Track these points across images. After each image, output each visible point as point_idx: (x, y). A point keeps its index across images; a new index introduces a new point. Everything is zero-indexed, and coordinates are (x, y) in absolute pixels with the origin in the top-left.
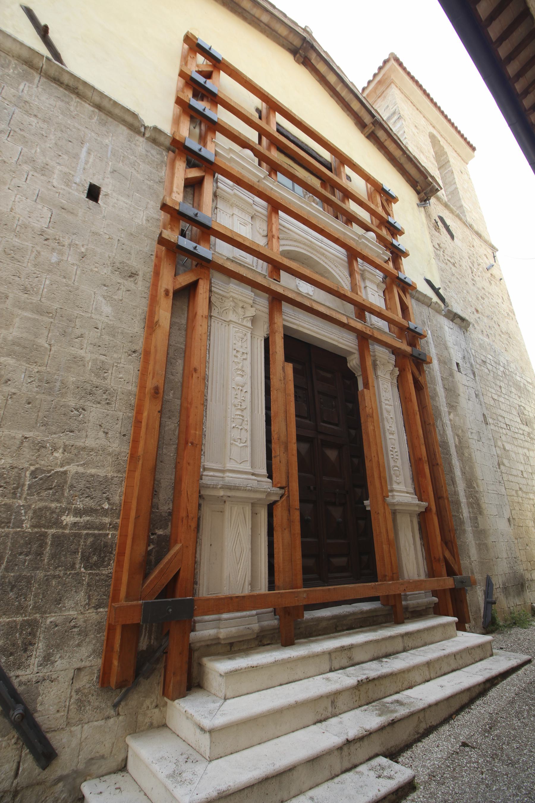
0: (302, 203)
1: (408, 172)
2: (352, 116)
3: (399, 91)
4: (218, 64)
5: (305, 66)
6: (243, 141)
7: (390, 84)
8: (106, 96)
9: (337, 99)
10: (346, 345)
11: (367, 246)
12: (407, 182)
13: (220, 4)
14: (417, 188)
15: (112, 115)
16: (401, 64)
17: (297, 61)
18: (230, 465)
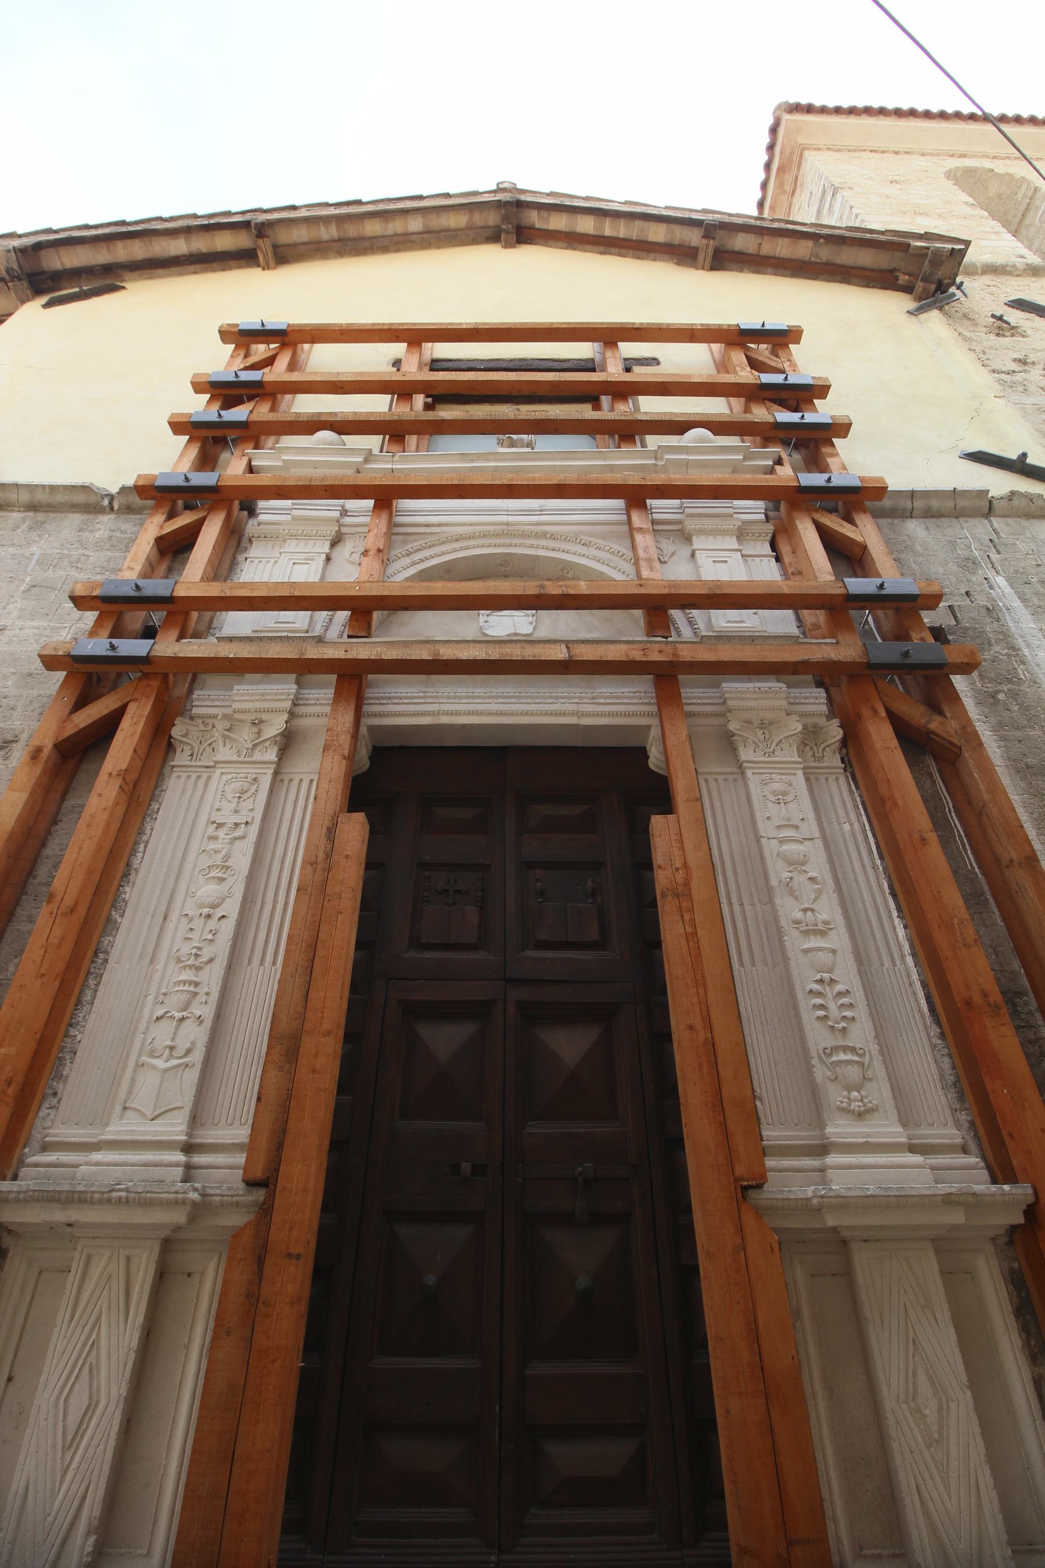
0: (472, 461)
1: (853, 268)
2: (664, 256)
3: (830, 153)
4: (286, 338)
5: (530, 244)
6: (307, 422)
7: (801, 155)
8: (36, 486)
9: (617, 250)
10: (610, 714)
11: (687, 464)
12: (867, 286)
13: (336, 258)
14: (900, 282)
15: (54, 507)
16: (809, 109)
17: (508, 245)
18: (117, 1129)
